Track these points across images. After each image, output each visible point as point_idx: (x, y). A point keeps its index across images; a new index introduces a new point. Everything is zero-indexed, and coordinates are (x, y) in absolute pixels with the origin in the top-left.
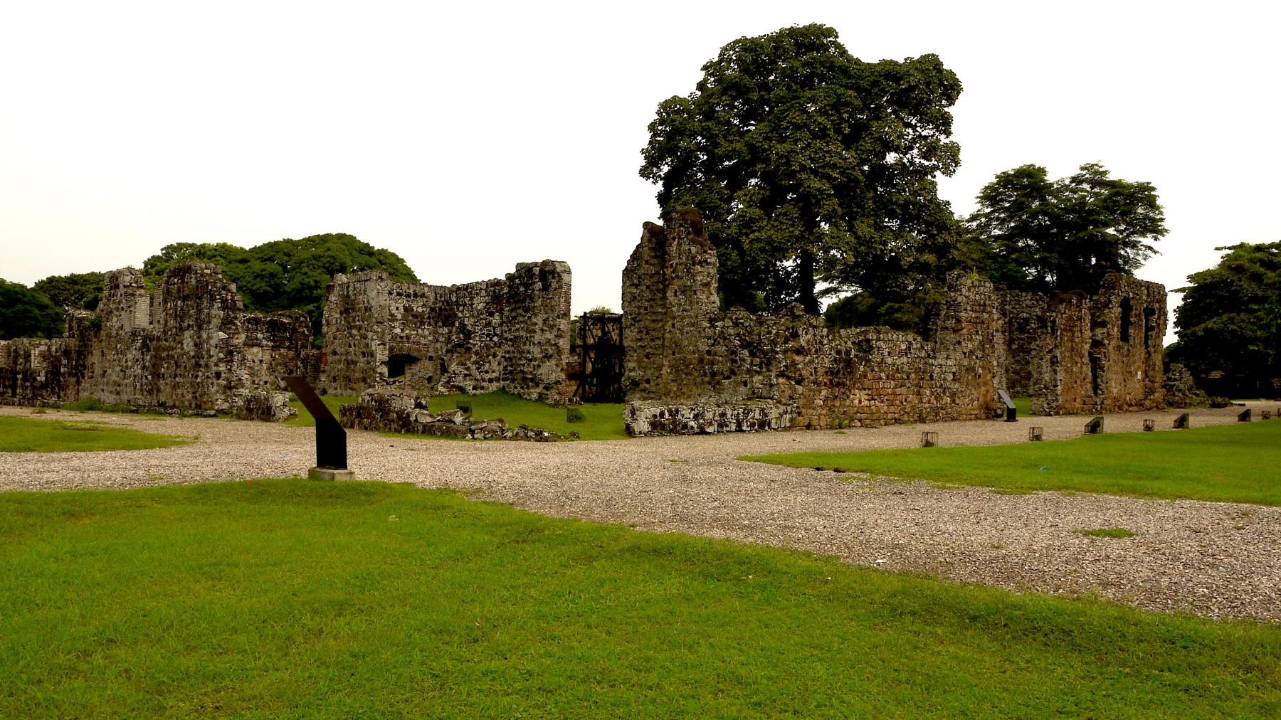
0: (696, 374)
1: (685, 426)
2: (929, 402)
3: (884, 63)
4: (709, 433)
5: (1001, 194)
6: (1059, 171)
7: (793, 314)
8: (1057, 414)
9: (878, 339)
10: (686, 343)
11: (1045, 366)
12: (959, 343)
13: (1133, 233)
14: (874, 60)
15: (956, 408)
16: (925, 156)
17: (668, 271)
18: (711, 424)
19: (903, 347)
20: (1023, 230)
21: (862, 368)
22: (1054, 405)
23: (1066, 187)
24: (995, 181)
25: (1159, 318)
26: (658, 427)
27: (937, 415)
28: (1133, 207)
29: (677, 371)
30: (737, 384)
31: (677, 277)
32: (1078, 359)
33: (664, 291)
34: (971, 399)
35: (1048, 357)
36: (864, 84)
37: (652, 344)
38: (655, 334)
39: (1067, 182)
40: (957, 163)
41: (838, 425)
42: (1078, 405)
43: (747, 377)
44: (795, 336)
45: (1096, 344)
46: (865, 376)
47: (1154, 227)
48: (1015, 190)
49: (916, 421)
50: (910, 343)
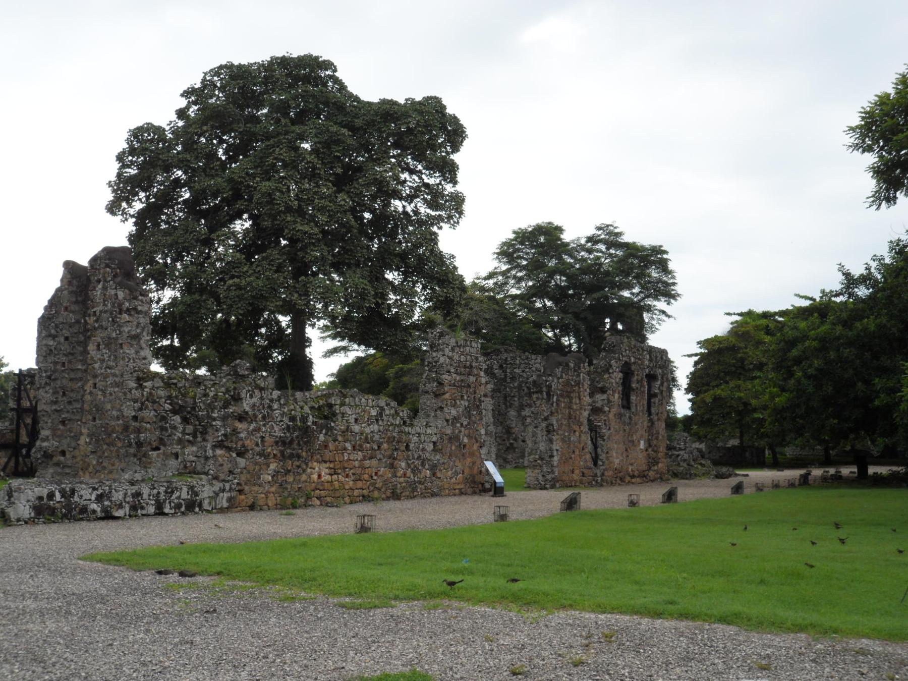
0: (120, 445)
1: (84, 510)
2: (405, 475)
3: (384, 102)
4: (167, 514)
5: (519, 250)
6: (575, 232)
7: (236, 374)
8: (553, 487)
9: (343, 404)
10: (109, 406)
11: (541, 435)
12: (441, 408)
13: (648, 297)
14: (375, 100)
15: (437, 482)
16: (433, 205)
17: (91, 320)
18: (120, 506)
19: (374, 413)
20: (540, 291)
21: (322, 437)
22: (549, 477)
23: (582, 247)
24: (512, 236)
25: (662, 384)
26: (44, 512)
27: (414, 490)
28: (644, 268)
29: (97, 441)
30: (166, 456)
31: (101, 327)
32: (576, 427)
33: (85, 344)
34: (450, 476)
35: (544, 425)
36: (358, 122)
37: (70, 407)
38: (72, 395)
39: (583, 241)
40: (461, 213)
41: (289, 504)
42: (576, 476)
43: (177, 448)
44: (237, 399)
45: (596, 410)
46: (326, 447)
47: (667, 292)
48: (532, 247)
49: (388, 498)
50: (382, 409)
